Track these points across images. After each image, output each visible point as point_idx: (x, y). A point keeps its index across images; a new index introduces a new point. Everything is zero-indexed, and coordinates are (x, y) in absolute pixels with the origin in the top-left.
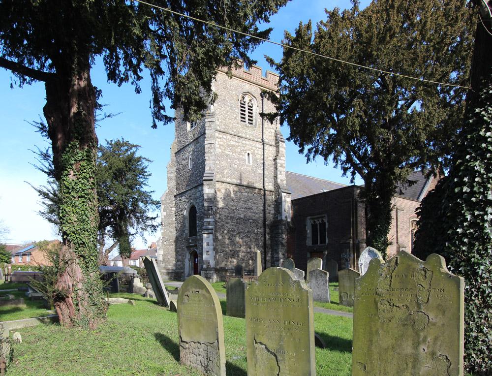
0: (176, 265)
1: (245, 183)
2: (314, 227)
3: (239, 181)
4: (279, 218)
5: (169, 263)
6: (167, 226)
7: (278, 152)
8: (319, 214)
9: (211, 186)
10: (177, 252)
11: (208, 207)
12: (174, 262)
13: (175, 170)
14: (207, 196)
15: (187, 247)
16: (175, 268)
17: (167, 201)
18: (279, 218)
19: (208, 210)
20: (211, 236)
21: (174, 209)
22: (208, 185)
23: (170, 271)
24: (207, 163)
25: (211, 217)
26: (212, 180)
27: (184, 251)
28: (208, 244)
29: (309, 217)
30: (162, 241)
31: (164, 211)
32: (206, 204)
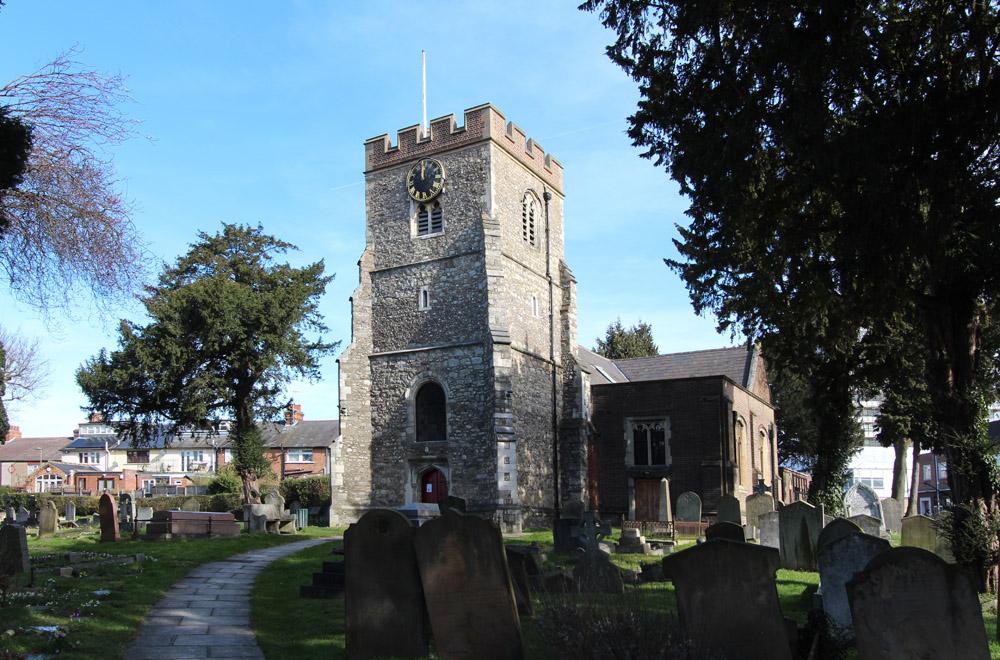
0: (372, 496)
1: (531, 351)
2: (640, 438)
3: (524, 346)
4: (574, 415)
5: (358, 491)
6: (354, 415)
7: (569, 298)
8: (653, 415)
9: (507, 355)
10: (376, 470)
11: (502, 392)
12: (369, 490)
13: (370, 305)
14: (500, 372)
15: (410, 461)
16: (369, 502)
17: (354, 366)
18: (574, 415)
19: (503, 398)
20: (513, 446)
21: (368, 382)
22: (501, 351)
23: (362, 508)
24: (490, 309)
25: (507, 410)
26: (509, 344)
27: (403, 468)
28: (507, 460)
29: (631, 418)
30: (341, 446)
31: (346, 385)
32: (498, 387)
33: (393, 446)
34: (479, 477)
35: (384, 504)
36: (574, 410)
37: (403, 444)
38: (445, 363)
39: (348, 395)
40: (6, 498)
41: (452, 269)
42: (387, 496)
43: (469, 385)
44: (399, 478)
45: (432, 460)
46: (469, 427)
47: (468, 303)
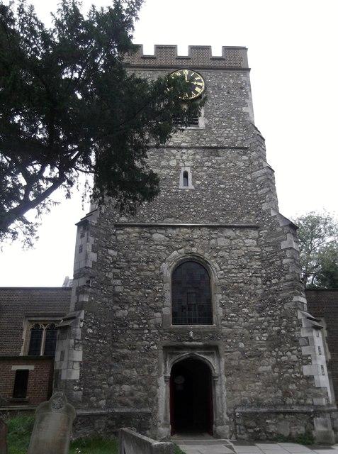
17: (102, 231)
27: (155, 356)
33: (143, 329)
34: (261, 369)
35: (126, 405)
36: (57, 325)
37: (157, 326)
38: (213, 241)
39: (93, 262)
40: (138, 4)
41: (217, 158)
42: (132, 394)
43: (242, 267)
44: (151, 370)
45: (194, 348)
46: (246, 310)
47: (237, 189)
